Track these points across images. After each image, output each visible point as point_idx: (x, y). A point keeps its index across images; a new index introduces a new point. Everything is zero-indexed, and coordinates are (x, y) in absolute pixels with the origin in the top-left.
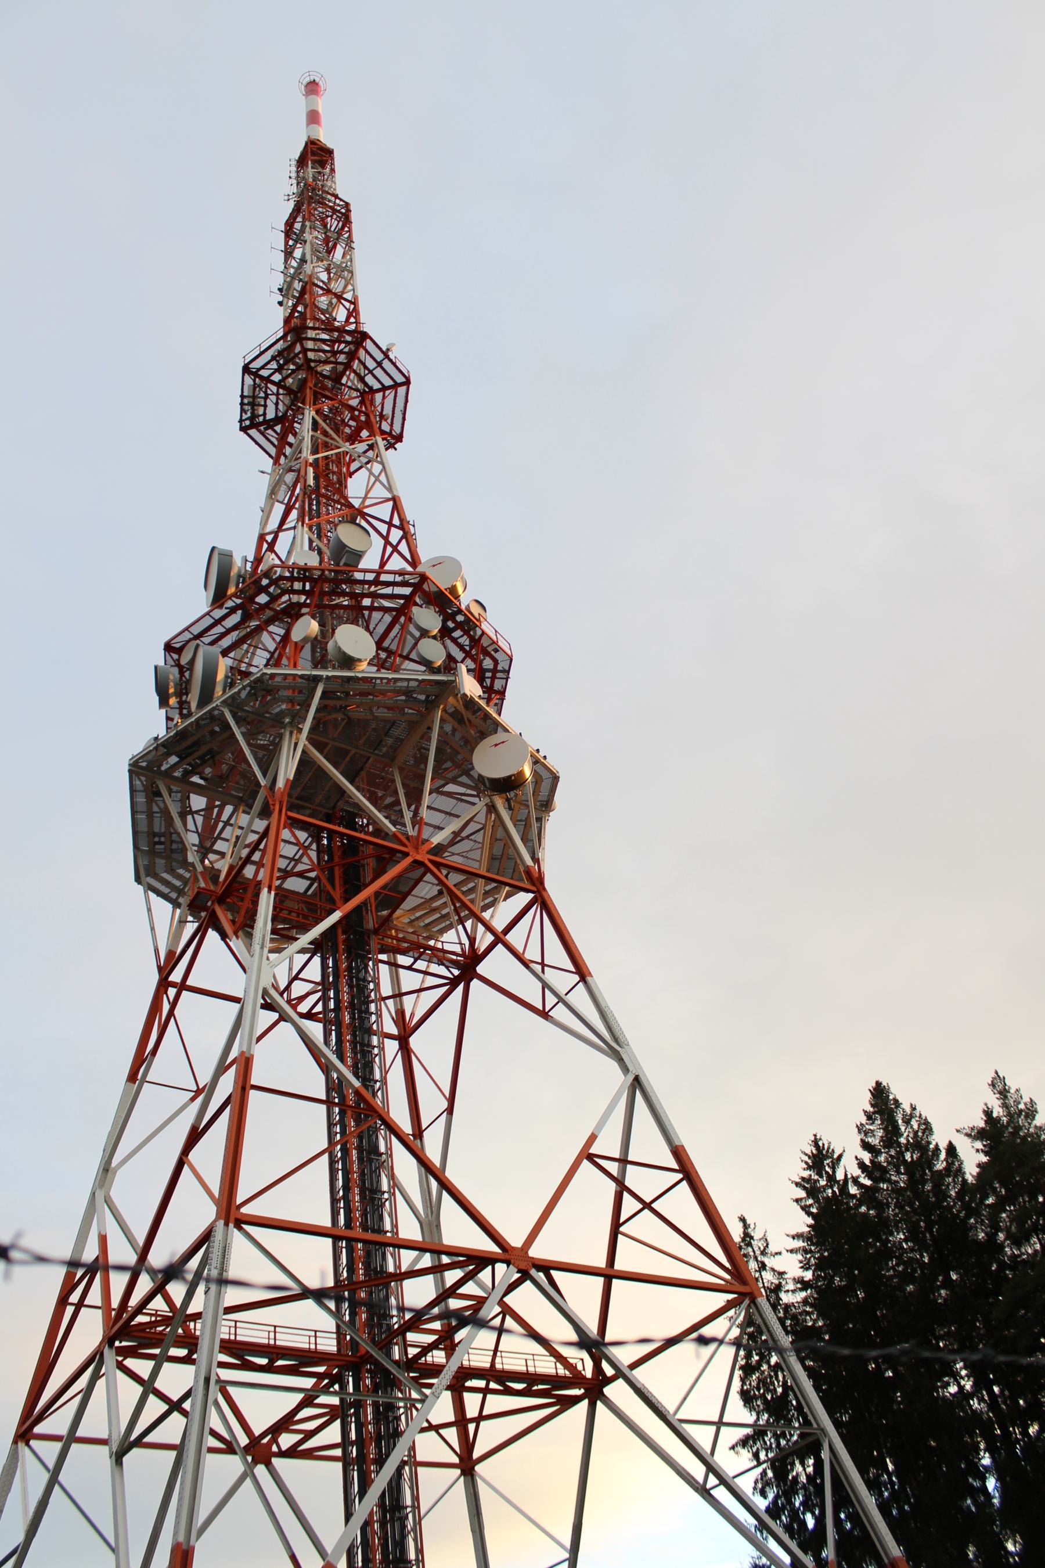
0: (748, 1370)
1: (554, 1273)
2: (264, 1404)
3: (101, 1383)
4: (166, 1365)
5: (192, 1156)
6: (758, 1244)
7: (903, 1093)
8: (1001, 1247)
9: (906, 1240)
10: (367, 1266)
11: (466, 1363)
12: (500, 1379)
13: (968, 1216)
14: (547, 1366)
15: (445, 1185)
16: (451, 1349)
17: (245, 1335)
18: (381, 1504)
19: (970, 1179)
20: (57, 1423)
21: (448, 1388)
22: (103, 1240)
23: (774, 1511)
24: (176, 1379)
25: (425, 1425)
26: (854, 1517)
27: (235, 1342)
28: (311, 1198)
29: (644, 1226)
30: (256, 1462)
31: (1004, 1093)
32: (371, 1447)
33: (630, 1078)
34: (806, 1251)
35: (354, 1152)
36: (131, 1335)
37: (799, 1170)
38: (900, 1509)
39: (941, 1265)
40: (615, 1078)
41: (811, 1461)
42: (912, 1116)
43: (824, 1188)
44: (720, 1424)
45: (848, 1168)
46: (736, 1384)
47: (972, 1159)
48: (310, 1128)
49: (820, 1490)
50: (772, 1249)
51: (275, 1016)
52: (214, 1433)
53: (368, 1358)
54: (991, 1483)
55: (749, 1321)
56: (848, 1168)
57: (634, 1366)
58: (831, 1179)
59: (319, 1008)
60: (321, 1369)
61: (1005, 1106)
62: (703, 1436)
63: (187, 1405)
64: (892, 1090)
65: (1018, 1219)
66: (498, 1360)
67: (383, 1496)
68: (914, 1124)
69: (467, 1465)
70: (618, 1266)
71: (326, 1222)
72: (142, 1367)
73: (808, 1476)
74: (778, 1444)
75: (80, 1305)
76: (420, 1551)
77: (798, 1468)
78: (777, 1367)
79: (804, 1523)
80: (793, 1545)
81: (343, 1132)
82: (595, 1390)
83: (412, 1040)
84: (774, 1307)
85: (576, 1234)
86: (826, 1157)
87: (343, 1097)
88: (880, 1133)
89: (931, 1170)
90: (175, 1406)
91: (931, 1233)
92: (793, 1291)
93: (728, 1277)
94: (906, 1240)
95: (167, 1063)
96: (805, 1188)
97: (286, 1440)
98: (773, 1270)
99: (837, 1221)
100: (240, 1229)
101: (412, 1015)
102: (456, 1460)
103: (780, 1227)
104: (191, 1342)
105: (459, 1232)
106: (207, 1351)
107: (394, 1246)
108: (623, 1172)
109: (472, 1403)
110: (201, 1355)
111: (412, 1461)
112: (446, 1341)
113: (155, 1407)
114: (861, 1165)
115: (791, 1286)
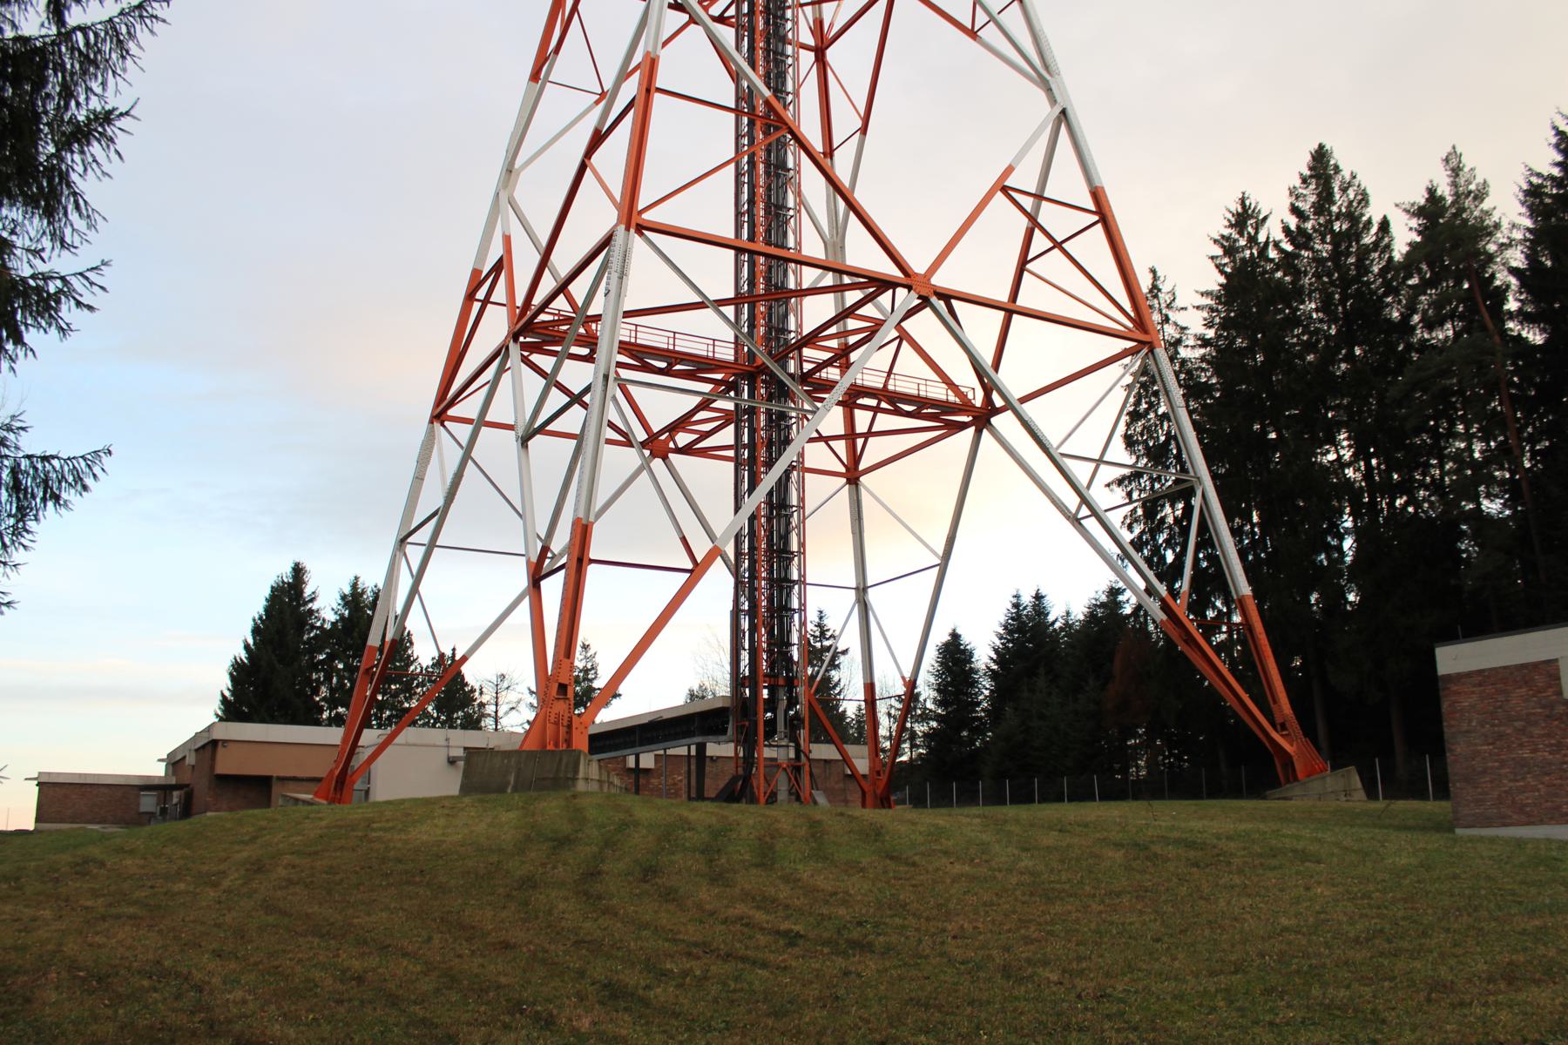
0: (1135, 416)
1: (954, 302)
2: (663, 403)
3: (506, 377)
4: (567, 362)
5: (595, 159)
6: (1164, 297)
7: (1346, 160)
8: (1414, 328)
9: (1317, 310)
10: (768, 280)
11: (859, 382)
12: (892, 400)
13: (1386, 294)
14: (939, 392)
15: (852, 206)
16: (846, 367)
17: (644, 339)
18: (769, 503)
19: (1397, 256)
20: (468, 407)
21: (839, 403)
22: (507, 240)
23: (1138, 544)
24: (576, 375)
25: (815, 435)
26: (1213, 560)
27: (636, 345)
28: (715, 207)
29: (1052, 265)
30: (653, 455)
31: (1456, 171)
32: (762, 450)
33: (1058, 110)
34: (1212, 310)
35: (761, 166)
36: (535, 333)
37: (1221, 228)
38: (1256, 556)
39: (1348, 337)
40: (1040, 109)
41: (1181, 506)
42: (1350, 185)
43: (1243, 248)
44: (1100, 461)
45: (1273, 231)
46: (1122, 428)
47: (1404, 236)
48: (718, 136)
49: (1185, 532)
50: (1178, 303)
51: (686, 17)
52: (611, 425)
53: (763, 369)
54: (1348, 543)
55: (1144, 371)
56: (1273, 231)
57: (1023, 400)
58: (1252, 240)
59: (732, 12)
60: (719, 376)
61: (1454, 185)
62: (1081, 472)
63: (587, 399)
64: (1335, 155)
65: (1437, 305)
66: (891, 382)
67: (770, 494)
68: (1351, 193)
69: (853, 476)
70: (1022, 301)
71: (728, 232)
72: (546, 362)
73: (1175, 518)
74: (1152, 488)
75: (486, 301)
76: (802, 545)
77: (1168, 510)
78: (1165, 417)
79: (1163, 558)
80: (1150, 574)
81: (751, 142)
82: (983, 418)
83: (829, 52)
84: (1172, 359)
85: (981, 268)
86: (1251, 217)
87: (752, 108)
88: (1313, 199)
89: (1358, 242)
90: (576, 399)
91: (1344, 307)
92: (1193, 347)
93: (1130, 325)
94: (1317, 310)
95: (570, 63)
96: (1223, 246)
97: (683, 439)
98: (1176, 324)
99: (1249, 287)
100: (641, 234)
101: (831, 25)
102: (843, 470)
103: (1191, 283)
104: (591, 341)
105: (863, 254)
106: (607, 352)
107: (797, 262)
108: (1037, 208)
109: (862, 420)
110: (601, 355)
111: (799, 466)
112: (842, 358)
113: (557, 399)
114: (1286, 230)
115: (1191, 342)
